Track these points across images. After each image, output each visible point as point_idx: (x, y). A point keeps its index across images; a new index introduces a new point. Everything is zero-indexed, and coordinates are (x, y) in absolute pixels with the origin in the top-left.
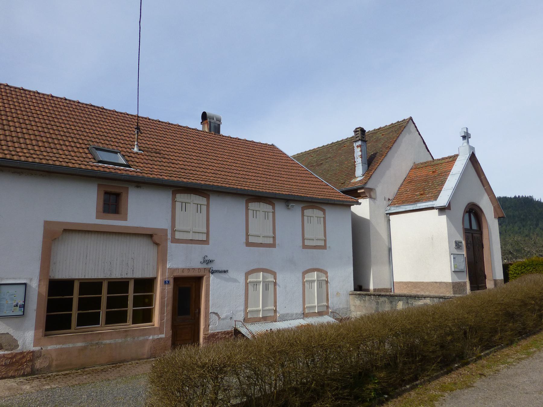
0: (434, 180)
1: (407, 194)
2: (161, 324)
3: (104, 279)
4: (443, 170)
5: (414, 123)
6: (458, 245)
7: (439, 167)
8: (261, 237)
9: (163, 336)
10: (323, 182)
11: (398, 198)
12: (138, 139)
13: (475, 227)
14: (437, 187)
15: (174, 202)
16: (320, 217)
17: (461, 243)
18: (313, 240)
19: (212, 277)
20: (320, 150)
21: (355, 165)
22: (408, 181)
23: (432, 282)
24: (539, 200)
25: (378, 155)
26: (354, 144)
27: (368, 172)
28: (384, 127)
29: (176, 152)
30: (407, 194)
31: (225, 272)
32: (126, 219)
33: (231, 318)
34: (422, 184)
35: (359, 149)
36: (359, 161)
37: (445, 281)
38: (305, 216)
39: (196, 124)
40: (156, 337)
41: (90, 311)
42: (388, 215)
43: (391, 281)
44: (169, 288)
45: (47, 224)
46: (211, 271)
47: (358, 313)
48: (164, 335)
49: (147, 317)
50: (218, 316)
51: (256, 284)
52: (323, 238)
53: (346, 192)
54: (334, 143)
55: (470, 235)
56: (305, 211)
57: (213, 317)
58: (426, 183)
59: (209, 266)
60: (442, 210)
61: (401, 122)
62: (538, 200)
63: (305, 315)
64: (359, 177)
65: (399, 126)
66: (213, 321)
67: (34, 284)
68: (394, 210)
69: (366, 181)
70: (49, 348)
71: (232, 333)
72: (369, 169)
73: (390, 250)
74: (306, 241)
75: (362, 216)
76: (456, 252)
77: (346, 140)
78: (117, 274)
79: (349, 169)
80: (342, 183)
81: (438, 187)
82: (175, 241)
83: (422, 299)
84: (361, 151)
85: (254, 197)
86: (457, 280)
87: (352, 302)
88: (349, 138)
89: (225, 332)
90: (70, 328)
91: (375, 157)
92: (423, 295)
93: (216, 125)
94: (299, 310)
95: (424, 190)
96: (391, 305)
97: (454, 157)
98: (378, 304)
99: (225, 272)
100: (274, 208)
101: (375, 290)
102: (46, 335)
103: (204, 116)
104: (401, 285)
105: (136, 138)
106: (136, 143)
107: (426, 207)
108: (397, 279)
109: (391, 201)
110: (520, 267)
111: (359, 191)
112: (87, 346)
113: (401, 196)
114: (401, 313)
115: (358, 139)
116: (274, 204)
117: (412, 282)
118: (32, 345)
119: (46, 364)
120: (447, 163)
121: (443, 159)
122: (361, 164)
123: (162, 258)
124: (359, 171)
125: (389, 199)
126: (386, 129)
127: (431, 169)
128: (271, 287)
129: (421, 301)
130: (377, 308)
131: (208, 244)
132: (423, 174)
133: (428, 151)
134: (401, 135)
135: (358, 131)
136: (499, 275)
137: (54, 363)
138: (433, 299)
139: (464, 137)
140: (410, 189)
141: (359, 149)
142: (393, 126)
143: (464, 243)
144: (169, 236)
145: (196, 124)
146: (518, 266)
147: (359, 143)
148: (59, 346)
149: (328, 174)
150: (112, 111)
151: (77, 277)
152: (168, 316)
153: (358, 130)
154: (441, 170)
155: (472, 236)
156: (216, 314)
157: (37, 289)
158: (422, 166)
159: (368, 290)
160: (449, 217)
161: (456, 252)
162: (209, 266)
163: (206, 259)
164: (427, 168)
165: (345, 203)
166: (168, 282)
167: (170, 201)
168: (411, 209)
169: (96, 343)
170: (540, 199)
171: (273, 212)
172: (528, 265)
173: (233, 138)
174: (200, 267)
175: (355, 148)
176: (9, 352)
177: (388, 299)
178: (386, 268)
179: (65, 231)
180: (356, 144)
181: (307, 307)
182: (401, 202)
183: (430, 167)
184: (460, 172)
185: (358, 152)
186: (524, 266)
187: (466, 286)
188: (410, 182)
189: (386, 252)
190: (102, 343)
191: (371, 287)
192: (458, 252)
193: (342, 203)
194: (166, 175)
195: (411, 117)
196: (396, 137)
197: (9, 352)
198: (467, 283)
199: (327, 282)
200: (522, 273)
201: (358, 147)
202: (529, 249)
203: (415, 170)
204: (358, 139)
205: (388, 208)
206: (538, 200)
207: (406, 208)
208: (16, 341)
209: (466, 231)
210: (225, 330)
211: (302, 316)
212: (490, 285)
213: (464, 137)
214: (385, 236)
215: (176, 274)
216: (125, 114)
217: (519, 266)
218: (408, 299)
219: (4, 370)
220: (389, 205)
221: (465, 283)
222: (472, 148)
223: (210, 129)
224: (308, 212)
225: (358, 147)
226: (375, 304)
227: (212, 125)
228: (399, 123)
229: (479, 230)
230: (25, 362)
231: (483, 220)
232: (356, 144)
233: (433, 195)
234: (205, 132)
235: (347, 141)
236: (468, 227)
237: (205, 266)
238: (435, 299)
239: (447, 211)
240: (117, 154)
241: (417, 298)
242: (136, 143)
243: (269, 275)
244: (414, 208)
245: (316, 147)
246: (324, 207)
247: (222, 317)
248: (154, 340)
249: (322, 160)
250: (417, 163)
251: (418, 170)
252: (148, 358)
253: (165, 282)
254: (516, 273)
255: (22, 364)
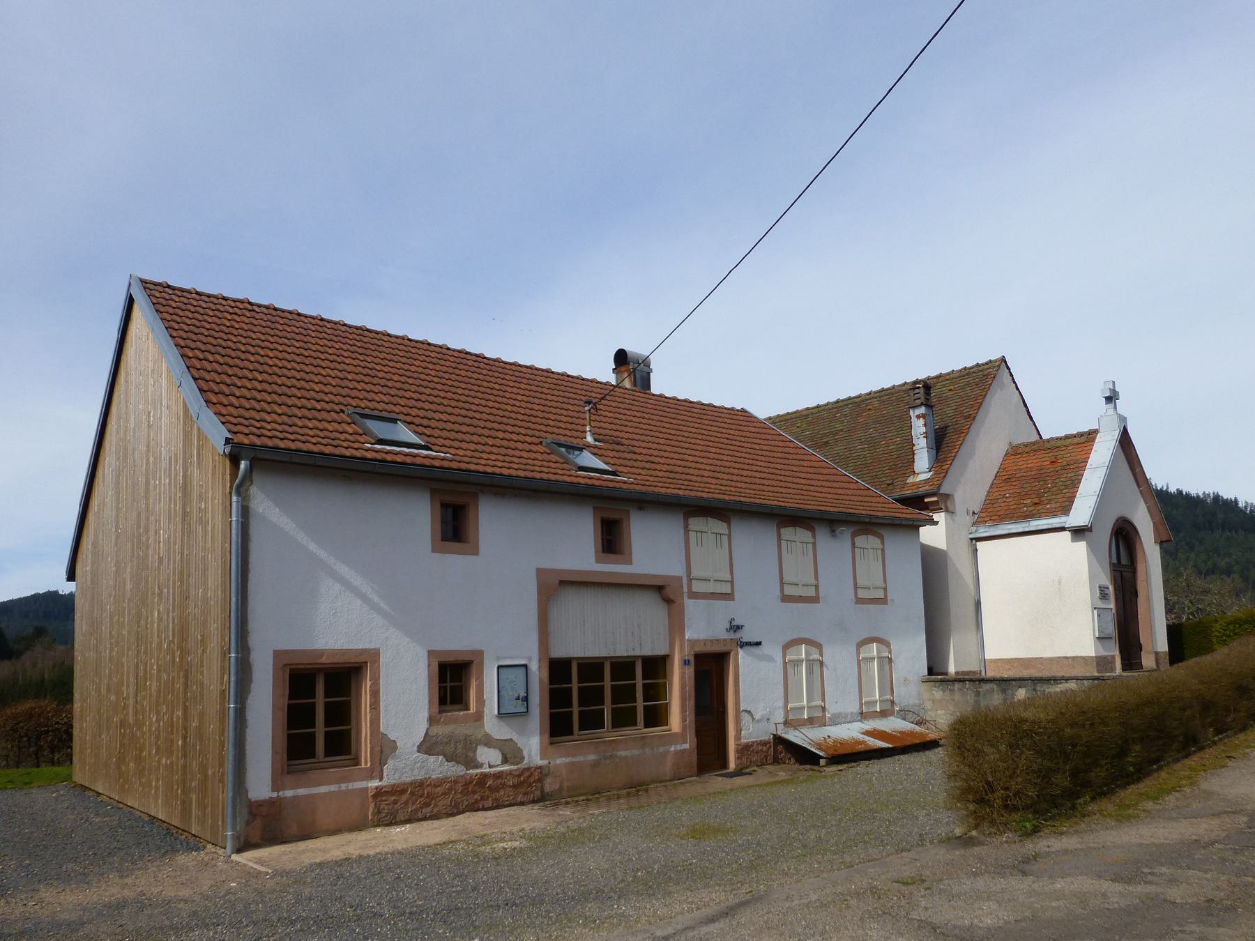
0: (1056, 477)
1: (1006, 504)
2: (684, 728)
3: (574, 658)
4: (1072, 458)
5: (1008, 369)
6: (1104, 596)
7: (1062, 453)
8: (712, 581)
9: (686, 746)
10: (858, 482)
11: (989, 510)
12: (590, 420)
13: (1124, 561)
14: (1064, 491)
15: (687, 529)
16: (702, 532)
17: (1108, 588)
18: (708, 582)
19: (741, 652)
20: (812, 414)
21: (913, 451)
22: (1004, 478)
23: (1059, 657)
24: (1165, 489)
25: (950, 430)
26: (911, 411)
27: (939, 464)
28: (948, 374)
29: (289, 375)
30: (1006, 504)
31: (759, 644)
32: (629, 562)
33: (768, 719)
34: (1034, 484)
35: (922, 421)
36: (921, 446)
37: (1083, 654)
38: (692, 531)
39: (605, 373)
40: (679, 747)
41: (623, 705)
42: (974, 542)
43: (980, 661)
44: (690, 671)
45: (541, 572)
46: (739, 643)
47: (939, 712)
48: (688, 745)
49: (656, 717)
50: (752, 716)
51: (798, 663)
52: (814, 582)
53: (905, 501)
54: (843, 401)
55: (1119, 574)
56: (856, 539)
57: (745, 717)
58: (1041, 483)
59: (737, 635)
60: (1079, 532)
61: (983, 365)
62: (1163, 487)
63: (863, 716)
64: (921, 473)
65: (981, 373)
66: (746, 724)
67: (534, 666)
68: (983, 531)
69: (940, 482)
70: (558, 761)
71: (770, 743)
72: (939, 458)
73: (978, 604)
74: (694, 583)
75: (930, 544)
76: (1100, 604)
77: (868, 397)
78: (622, 650)
79: (894, 457)
80: (889, 484)
81: (1066, 491)
82: (695, 595)
83: (1061, 683)
84: (925, 425)
85: (691, 509)
86: (1103, 653)
87: (926, 695)
88: (875, 392)
89: (761, 741)
90: (571, 733)
91: (946, 434)
92: (1063, 676)
93: (645, 374)
94: (855, 708)
95: (1039, 496)
96: (1004, 695)
97: (1089, 434)
98: (979, 695)
99: (759, 644)
100: (814, 536)
101: (957, 673)
102: (551, 744)
103: (621, 358)
104: (999, 665)
105: (588, 418)
106: (588, 428)
107: (1050, 527)
108: (989, 655)
109: (976, 516)
110: (1233, 625)
111: (926, 500)
112: (601, 759)
113: (995, 506)
114: (1025, 704)
115: (918, 402)
116: (883, 536)
117: (1021, 659)
118: (539, 757)
119: (556, 786)
120: (1077, 447)
121: (1067, 437)
122: (926, 449)
123: (676, 624)
124: (922, 461)
125: (974, 513)
126: (954, 378)
127: (1047, 455)
128: (817, 668)
129: (1061, 686)
130: (976, 701)
131: (733, 599)
132: (1033, 465)
133: (1031, 418)
134: (989, 392)
135: (919, 388)
136: (1162, 644)
137: (565, 784)
138: (1082, 681)
139: (1109, 399)
140: (1012, 494)
141: (922, 421)
142: (966, 372)
143: (1111, 588)
144: (685, 589)
145: (605, 373)
146: (1229, 624)
147: (922, 410)
148: (569, 760)
149: (850, 465)
150: (159, 284)
151: (576, 656)
152: (691, 717)
153: (918, 386)
154: (1067, 459)
155: (1122, 576)
156: (749, 712)
157: (537, 673)
158: (1027, 449)
159: (946, 674)
160: (1090, 545)
161: (1100, 604)
162: (737, 635)
163: (734, 623)
164: (1038, 453)
165: (904, 523)
166: (689, 661)
167: (682, 531)
168: (1021, 530)
169: (610, 756)
170: (1167, 484)
171: (882, 550)
172: (1246, 622)
173: (454, 350)
174: (725, 637)
175: (914, 419)
176: (516, 767)
177: (999, 686)
178: (971, 636)
179: (563, 583)
180: (914, 412)
181: (867, 703)
182: (997, 517)
183: (1043, 452)
184: (1107, 464)
185: (919, 428)
186: (1239, 623)
187: (1115, 663)
188: (1007, 481)
189: (972, 608)
190: (616, 756)
191: (952, 669)
192: (1103, 603)
193: (911, 523)
194: (315, 442)
195: (1004, 357)
196: (981, 397)
197: (516, 767)
198: (1116, 657)
199: (890, 660)
200: (1235, 634)
201: (918, 417)
202: (1176, 598)
203: (1013, 457)
204: (918, 402)
205: (974, 529)
206: (1163, 487)
207: (1010, 529)
208: (520, 750)
209: (1115, 569)
210: (762, 739)
211: (859, 718)
212: (1148, 661)
213: (1109, 399)
214: (969, 580)
215: (700, 649)
216: (218, 299)
217: (1231, 624)
218: (1035, 685)
219: (512, 793)
220: (974, 524)
221: (1113, 657)
222: (1123, 419)
223: (635, 384)
224: (860, 539)
225: (918, 417)
226: (973, 695)
227: (638, 376)
228: (980, 368)
229: (1130, 564)
230: (533, 782)
231: (1138, 547)
232: (914, 412)
233: (1059, 504)
234: (193, 291)
235: (870, 399)
236: (1115, 560)
237: (732, 635)
238: (1085, 682)
239: (1087, 533)
240: (397, 423)
241: (1052, 682)
242: (588, 428)
243: (813, 648)
244: (1027, 530)
245: (800, 406)
246: (882, 531)
247: (757, 717)
248: (676, 752)
249: (825, 435)
250: (1015, 443)
251: (1019, 456)
252: (670, 780)
253: (685, 661)
254: (1226, 636)
255: (530, 785)
